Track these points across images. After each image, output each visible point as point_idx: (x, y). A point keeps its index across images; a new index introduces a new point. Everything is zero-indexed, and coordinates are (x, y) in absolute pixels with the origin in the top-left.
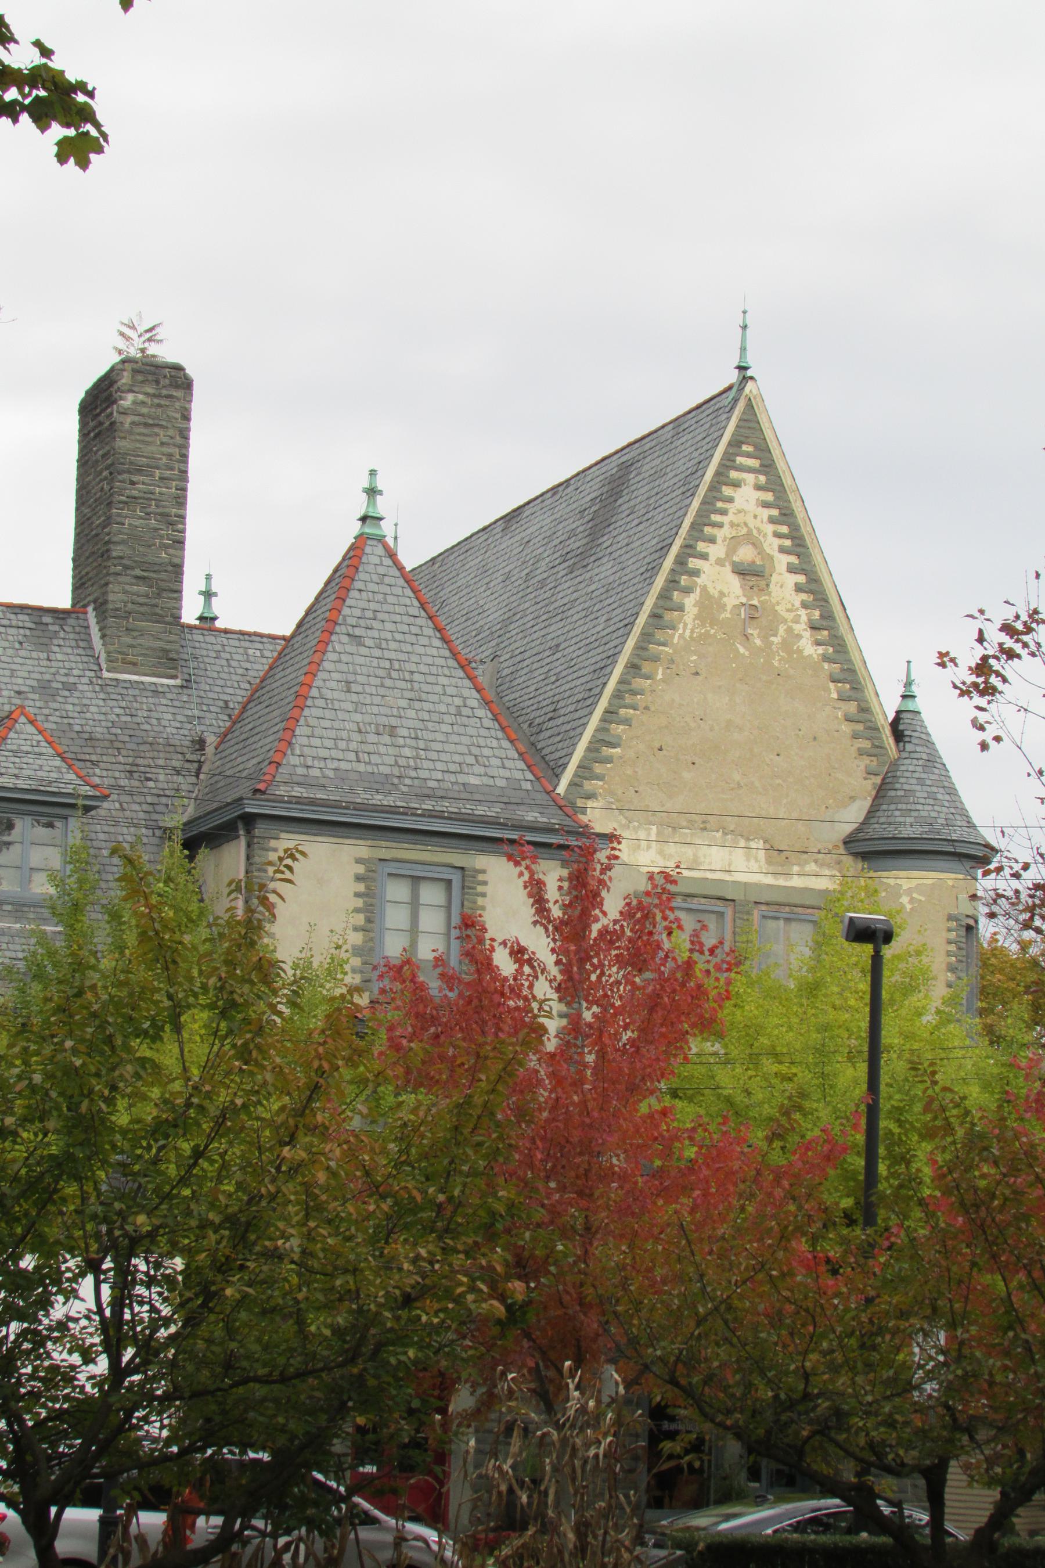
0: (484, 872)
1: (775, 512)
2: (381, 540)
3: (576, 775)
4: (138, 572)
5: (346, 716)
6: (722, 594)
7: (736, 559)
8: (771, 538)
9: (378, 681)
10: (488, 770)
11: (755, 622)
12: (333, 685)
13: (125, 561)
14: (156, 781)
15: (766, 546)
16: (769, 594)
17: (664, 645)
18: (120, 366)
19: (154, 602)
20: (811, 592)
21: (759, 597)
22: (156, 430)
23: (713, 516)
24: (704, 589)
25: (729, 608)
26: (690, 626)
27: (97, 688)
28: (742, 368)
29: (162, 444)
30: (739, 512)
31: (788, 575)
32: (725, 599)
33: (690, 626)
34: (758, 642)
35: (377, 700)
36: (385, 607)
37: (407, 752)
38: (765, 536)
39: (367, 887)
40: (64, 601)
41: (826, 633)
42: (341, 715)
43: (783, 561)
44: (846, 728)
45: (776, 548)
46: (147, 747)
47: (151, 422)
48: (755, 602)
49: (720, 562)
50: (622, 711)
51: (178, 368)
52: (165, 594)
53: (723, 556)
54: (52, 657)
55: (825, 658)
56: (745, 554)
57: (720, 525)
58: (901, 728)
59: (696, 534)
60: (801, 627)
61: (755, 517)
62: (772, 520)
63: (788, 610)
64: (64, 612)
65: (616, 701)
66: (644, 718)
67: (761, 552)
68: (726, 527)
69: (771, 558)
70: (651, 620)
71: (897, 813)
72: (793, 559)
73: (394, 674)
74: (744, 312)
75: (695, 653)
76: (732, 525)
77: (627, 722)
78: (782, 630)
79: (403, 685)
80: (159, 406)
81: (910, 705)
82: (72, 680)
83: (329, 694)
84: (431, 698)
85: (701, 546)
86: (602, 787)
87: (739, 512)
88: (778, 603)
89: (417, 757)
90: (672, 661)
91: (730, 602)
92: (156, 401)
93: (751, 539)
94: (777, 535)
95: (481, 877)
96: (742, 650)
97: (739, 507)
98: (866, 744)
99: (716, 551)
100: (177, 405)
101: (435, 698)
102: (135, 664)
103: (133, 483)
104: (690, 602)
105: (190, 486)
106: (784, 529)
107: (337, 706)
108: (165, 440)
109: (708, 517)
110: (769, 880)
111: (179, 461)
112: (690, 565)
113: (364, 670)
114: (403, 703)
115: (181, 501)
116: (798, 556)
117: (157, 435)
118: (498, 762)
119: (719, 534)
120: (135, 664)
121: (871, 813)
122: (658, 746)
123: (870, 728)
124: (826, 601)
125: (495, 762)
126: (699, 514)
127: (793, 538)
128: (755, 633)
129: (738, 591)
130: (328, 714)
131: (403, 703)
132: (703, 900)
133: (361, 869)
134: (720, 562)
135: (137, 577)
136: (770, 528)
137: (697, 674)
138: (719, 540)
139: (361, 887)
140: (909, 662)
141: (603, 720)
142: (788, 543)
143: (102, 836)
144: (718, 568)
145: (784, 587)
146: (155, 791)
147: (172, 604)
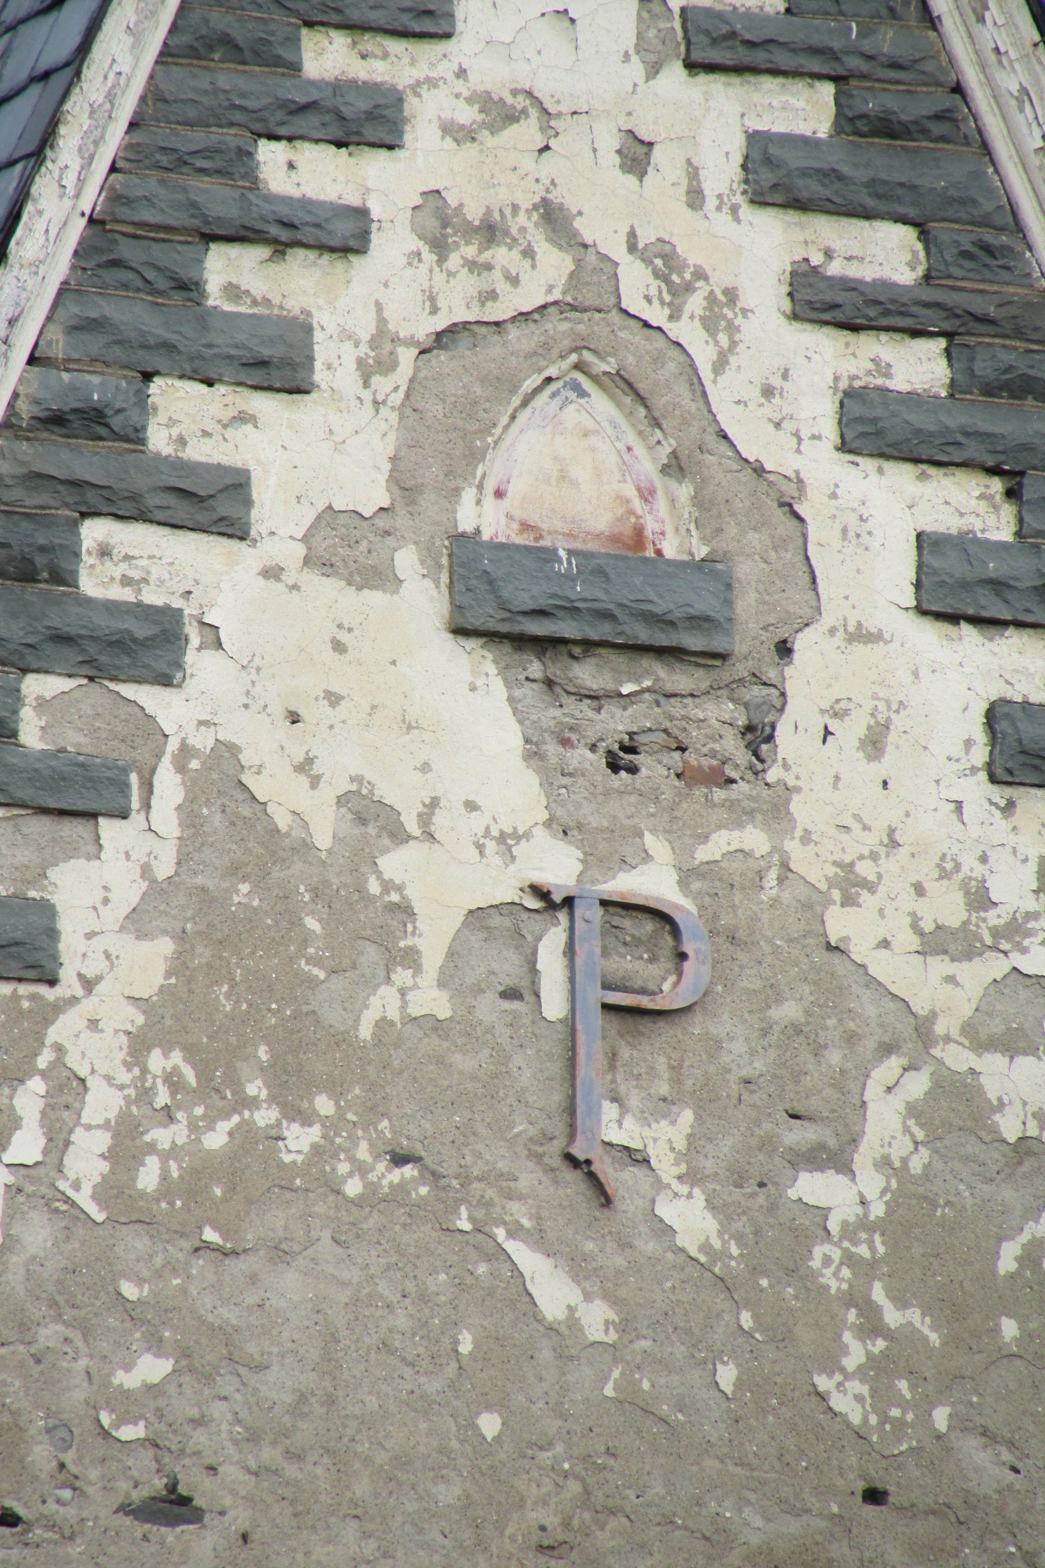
1: (805, 111)
6: (371, 817)
7: (481, 516)
8: (771, 332)
11: (653, 1052)
15: (731, 400)
16: (776, 811)
18: (228, 372)
21: (687, 835)
23: (270, 155)
24: (220, 778)
25: (434, 935)
26: (102, 1103)
30: (500, 113)
31: (929, 638)
32: (395, 863)
33: (102, 1103)
34: (691, 1219)
38: (723, 311)
43: (881, 522)
45: (821, 415)
48: (654, 881)
49: (345, 548)
53: (369, 493)
56: (564, 474)
57: (338, 235)
59: (131, 314)
61: (637, 154)
62: (776, 178)
63: (935, 943)
68: (393, 243)
75: (148, 1324)
76: (441, 225)
85: (185, 419)
87: (500, 113)
88: (851, 886)
91: (443, 885)
93: (603, 344)
94: (826, 303)
96: (553, 1292)
97: (493, 74)
106: (885, 253)
109: (239, 165)
112: (95, 582)
119: (335, 304)
126: (154, 142)
127: (957, 331)
128: (665, 1139)
129: (517, 794)
134: (345, 548)
136: (763, 248)
137: (175, 1506)
138: (334, 362)
142: (918, 367)
144: (327, 592)
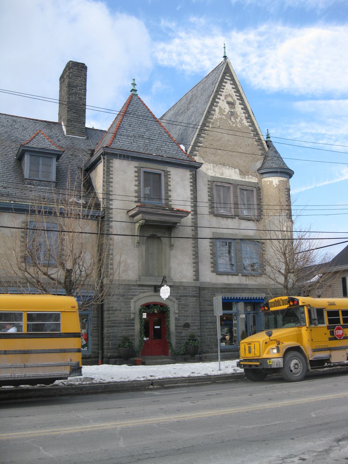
0: (170, 172)
1: (235, 90)
2: (136, 95)
3: (221, 78)
4: (74, 111)
5: (130, 132)
9: (138, 125)
10: (169, 147)
11: (232, 116)
12: (126, 125)
13: (71, 108)
14: (79, 157)
17: (211, 119)
19: (78, 118)
20: (245, 110)
22: (78, 77)
23: (223, 83)
24: (220, 107)
27: (64, 138)
28: (225, 57)
29: (80, 81)
35: (138, 129)
36: (138, 109)
37: (147, 141)
39: (138, 174)
40: (56, 120)
41: (249, 120)
42: (128, 132)
43: (238, 102)
44: (256, 143)
46: (77, 150)
47: (76, 75)
48: (232, 111)
50: (202, 135)
51: (84, 64)
52: (81, 117)
54: (52, 131)
55: (250, 126)
56: (230, 99)
57: (223, 92)
58: (269, 144)
60: (243, 118)
64: (56, 123)
65: (200, 132)
66: (208, 137)
67: (233, 99)
69: (235, 101)
70: (207, 113)
71: (270, 163)
72: (240, 102)
73: (142, 124)
74: (224, 44)
77: (203, 137)
78: (239, 118)
79: (145, 126)
80: (79, 72)
81: (269, 139)
82: (57, 136)
83: (125, 127)
84: (152, 130)
86: (198, 153)
89: (150, 143)
90: (213, 123)
92: (78, 71)
94: (236, 96)
95: (169, 173)
98: (261, 147)
99: (222, 98)
100: (83, 72)
101: (153, 130)
102: (74, 133)
103: (73, 90)
104: (217, 109)
105: (87, 92)
106: (238, 94)
107: (127, 129)
108: (81, 80)
110: (240, 179)
111: (84, 85)
113: (134, 122)
114: (145, 130)
115: (85, 95)
116: (242, 101)
117: (78, 79)
118: (171, 146)
119: (223, 94)
120: (74, 133)
121: (263, 164)
122: (211, 144)
123: (261, 144)
124: (249, 112)
125: (170, 145)
127: (240, 97)
130: (125, 131)
131: (145, 130)
132: (225, 184)
133: (136, 169)
134: (223, 101)
135: (73, 112)
136: (235, 94)
138: (223, 95)
139: (137, 174)
140: (268, 130)
141: (197, 136)
142: (239, 98)
143: (64, 168)
145: (239, 109)
146: (78, 159)
147: (83, 119)
